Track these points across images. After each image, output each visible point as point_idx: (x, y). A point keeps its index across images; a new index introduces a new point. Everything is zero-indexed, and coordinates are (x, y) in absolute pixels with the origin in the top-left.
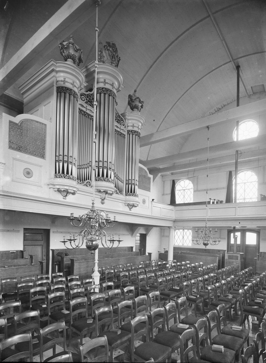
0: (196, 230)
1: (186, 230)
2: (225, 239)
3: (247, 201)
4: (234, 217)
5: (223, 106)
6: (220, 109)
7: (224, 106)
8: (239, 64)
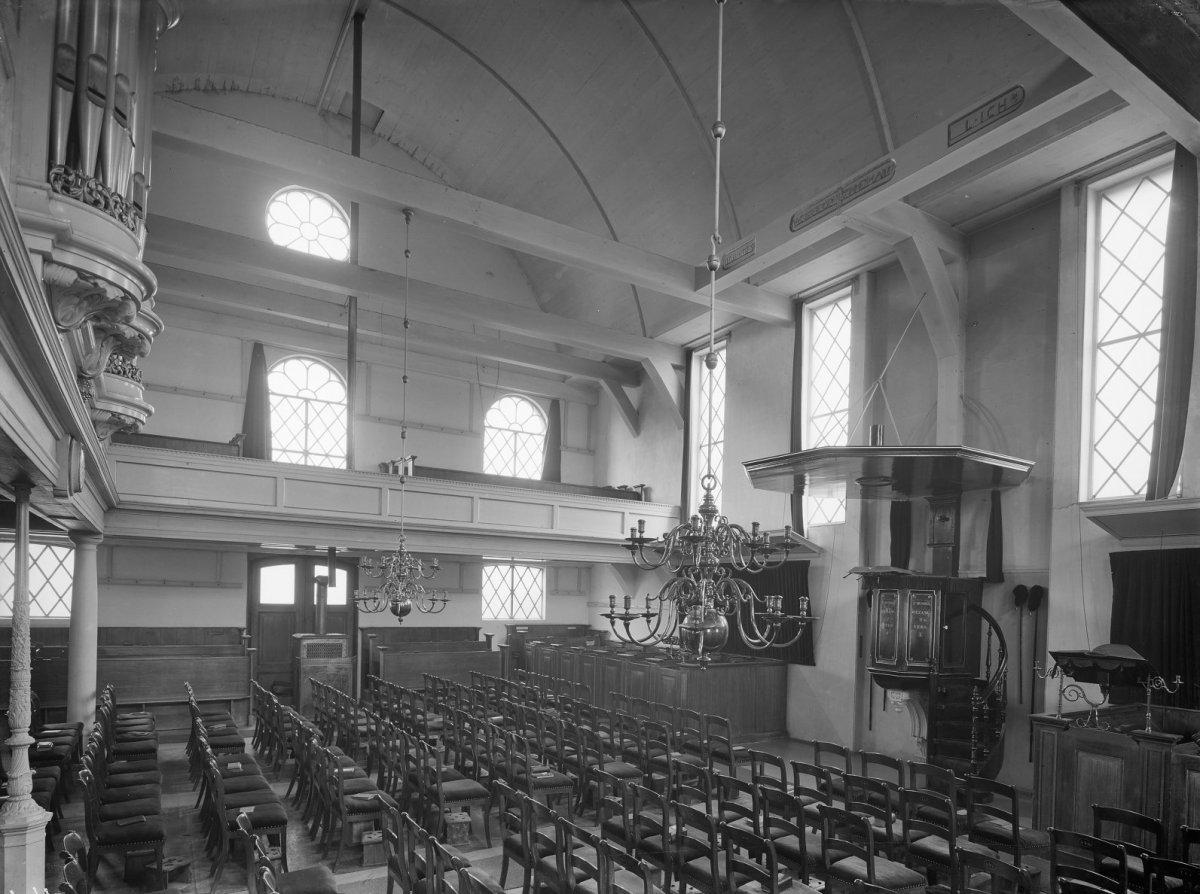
0: (557, 573)
1: (520, 569)
2: (238, 586)
3: (315, 461)
4: (267, 509)
5: (228, 87)
6: (214, 89)
7: (233, 89)
8: (366, 10)
